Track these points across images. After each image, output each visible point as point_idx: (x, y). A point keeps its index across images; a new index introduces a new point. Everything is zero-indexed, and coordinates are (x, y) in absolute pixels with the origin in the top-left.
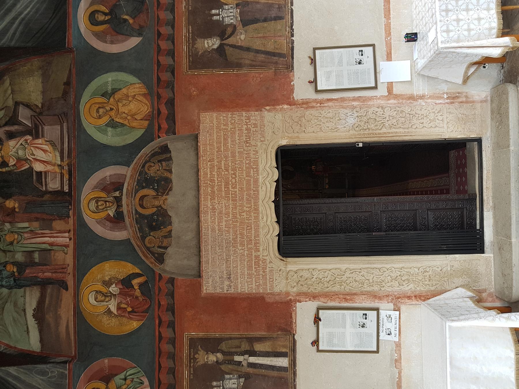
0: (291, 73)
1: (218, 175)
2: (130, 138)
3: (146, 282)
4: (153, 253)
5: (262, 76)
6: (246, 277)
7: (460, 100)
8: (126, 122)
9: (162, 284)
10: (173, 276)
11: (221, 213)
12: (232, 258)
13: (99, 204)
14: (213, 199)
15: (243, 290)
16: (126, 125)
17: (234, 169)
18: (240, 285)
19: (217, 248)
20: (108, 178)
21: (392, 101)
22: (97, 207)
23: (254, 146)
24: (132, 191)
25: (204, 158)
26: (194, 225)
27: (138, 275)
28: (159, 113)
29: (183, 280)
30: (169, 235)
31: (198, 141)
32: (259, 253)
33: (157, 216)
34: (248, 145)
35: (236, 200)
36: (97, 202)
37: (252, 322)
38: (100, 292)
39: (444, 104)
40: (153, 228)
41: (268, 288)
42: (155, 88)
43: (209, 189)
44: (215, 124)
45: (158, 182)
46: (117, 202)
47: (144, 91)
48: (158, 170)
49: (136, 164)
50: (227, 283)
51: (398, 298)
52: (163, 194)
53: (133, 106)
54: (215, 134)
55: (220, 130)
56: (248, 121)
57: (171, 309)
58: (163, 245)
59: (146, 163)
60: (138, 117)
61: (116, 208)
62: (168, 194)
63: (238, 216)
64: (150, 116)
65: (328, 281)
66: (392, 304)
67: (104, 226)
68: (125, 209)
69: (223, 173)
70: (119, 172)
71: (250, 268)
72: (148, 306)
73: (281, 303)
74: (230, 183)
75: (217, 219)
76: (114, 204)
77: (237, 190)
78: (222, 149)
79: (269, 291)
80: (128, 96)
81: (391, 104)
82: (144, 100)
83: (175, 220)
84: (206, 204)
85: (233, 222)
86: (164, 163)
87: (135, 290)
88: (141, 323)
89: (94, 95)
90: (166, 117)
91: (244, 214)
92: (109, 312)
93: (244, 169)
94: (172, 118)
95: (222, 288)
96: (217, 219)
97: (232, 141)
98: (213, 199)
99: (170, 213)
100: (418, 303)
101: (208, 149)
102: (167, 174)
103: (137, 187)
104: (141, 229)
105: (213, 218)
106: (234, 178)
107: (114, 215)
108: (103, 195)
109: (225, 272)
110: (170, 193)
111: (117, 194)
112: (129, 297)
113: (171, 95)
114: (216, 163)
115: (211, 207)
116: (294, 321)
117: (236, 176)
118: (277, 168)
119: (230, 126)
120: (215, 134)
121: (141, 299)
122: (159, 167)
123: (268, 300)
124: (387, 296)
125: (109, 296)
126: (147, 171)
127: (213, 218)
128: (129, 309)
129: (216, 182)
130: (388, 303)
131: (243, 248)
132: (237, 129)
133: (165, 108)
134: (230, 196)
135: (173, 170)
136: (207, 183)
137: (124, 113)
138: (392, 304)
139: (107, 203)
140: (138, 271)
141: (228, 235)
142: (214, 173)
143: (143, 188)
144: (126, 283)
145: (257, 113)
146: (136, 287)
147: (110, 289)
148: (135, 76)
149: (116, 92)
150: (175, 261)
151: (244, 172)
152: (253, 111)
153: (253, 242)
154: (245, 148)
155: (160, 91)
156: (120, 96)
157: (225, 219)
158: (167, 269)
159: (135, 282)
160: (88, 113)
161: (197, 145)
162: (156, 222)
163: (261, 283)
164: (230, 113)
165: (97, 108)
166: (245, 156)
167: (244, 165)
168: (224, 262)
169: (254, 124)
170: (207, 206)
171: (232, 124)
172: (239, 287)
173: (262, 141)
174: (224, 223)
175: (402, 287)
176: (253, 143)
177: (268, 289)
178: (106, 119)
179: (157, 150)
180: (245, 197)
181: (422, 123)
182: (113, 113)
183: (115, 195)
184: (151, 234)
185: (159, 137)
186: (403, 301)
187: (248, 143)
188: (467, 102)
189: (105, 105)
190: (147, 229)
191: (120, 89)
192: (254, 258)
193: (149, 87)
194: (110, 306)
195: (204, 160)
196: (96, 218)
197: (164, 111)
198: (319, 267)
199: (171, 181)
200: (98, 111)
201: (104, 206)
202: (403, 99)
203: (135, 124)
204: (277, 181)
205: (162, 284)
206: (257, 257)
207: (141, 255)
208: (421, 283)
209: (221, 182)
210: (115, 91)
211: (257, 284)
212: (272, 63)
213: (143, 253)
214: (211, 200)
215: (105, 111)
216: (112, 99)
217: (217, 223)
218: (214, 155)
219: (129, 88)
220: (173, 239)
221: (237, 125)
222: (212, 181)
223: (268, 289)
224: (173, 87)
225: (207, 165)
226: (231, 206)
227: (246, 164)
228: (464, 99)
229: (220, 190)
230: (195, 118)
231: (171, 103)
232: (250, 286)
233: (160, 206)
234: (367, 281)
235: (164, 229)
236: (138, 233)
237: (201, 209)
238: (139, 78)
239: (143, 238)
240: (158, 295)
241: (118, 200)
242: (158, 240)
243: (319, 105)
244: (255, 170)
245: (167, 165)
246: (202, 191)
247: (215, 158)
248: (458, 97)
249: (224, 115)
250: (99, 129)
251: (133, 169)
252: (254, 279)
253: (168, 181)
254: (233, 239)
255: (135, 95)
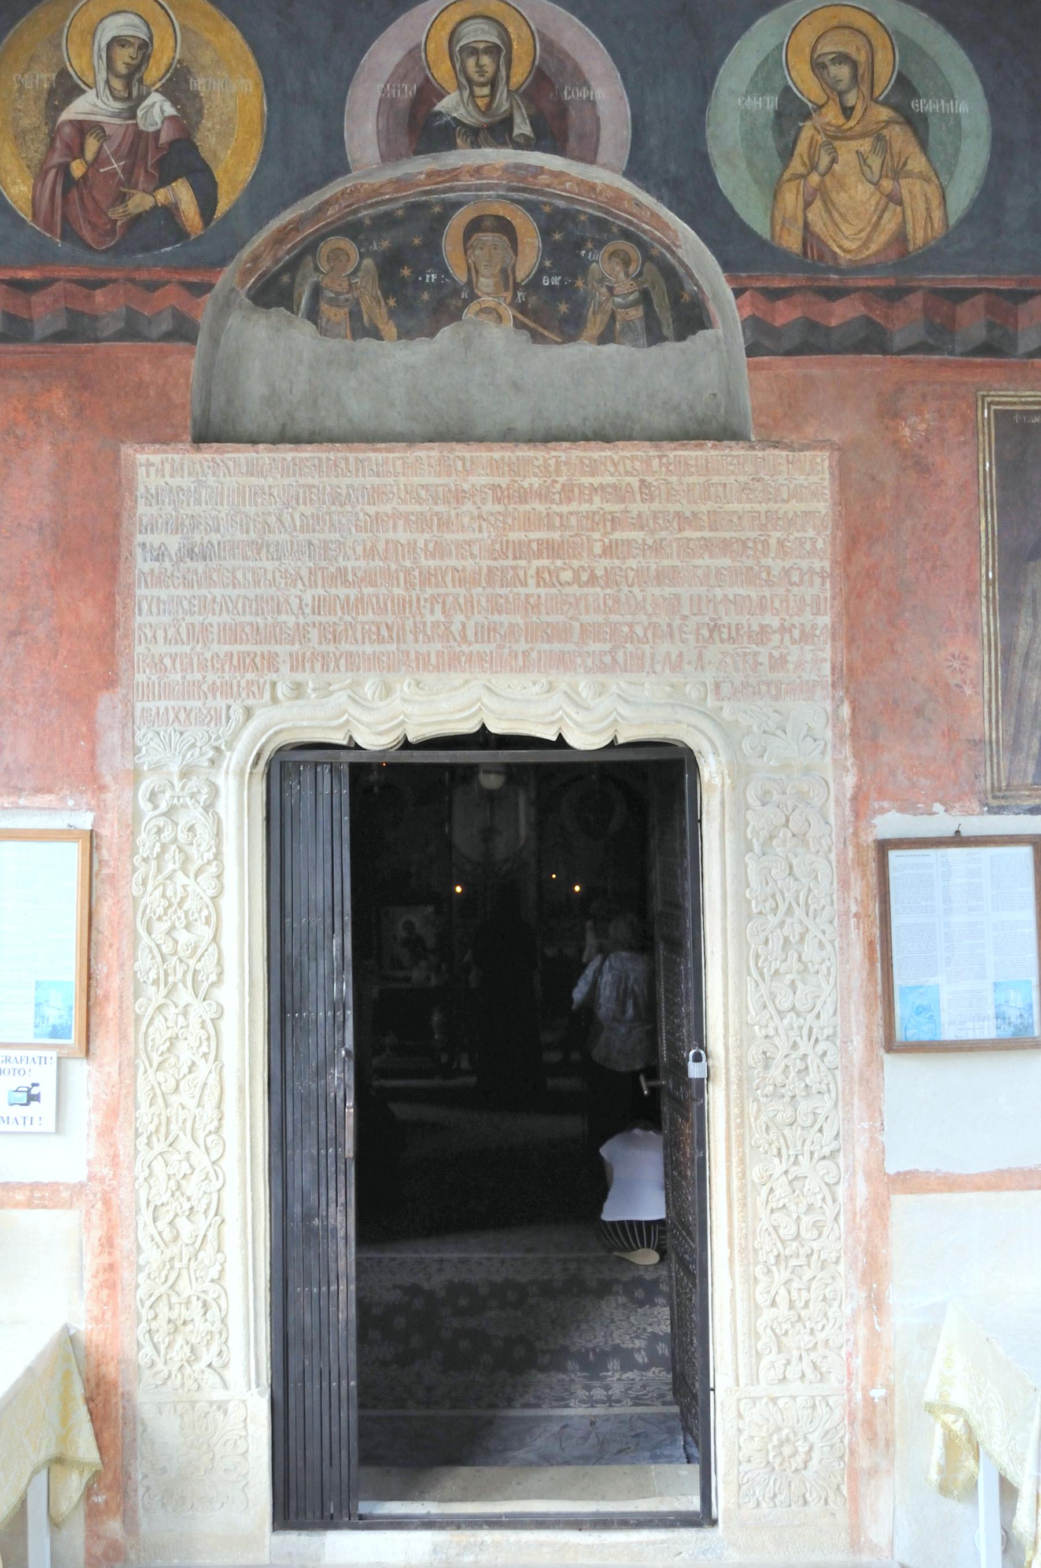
0: (975, 806)
1: (590, 516)
2: (736, 183)
3: (181, 234)
4: (293, 266)
5: (968, 691)
6: (197, 619)
7: (863, 1449)
8: (796, 165)
9: (171, 297)
10: (202, 339)
11: (444, 524)
12: (270, 565)
13: (486, 60)
14: (499, 494)
15: (145, 606)
16: (786, 166)
17: (610, 578)
18: (163, 594)
19: (308, 510)
20: (583, 94)
21: (862, 1189)
22: (475, 52)
23: (700, 657)
24: (532, 191)
25: (655, 462)
26: (396, 420)
27: (207, 199)
28: (832, 294)
29: (187, 376)
30: (362, 329)
31: (720, 440)
32: (285, 669)
33: (439, 285)
34: (706, 633)
35: (490, 583)
36: (493, 50)
37: (21, 640)
38: (145, 59)
39: (849, 1390)
40: (389, 270)
41: (152, 705)
42: (928, 280)
43: (536, 482)
44: (786, 507)
45: (565, 291)
46: (491, 129)
47: (918, 237)
48: (611, 289)
49: (638, 204)
50: (173, 542)
51: (107, 1203)
52: (522, 308)
53: (858, 195)
54: (748, 507)
55: (763, 527)
56: (796, 633)
57: (77, 330)
58: (324, 306)
59: (640, 244)
60: (816, 214)
61: (468, 120)
62: (519, 325)
63: (429, 591)
64: (821, 257)
65: (175, 934)
66: (83, 1178)
67: (400, 75)
68: (463, 157)
69: (596, 535)
70: (606, 134)
71: (232, 633)
72: (90, 241)
73: (93, 754)
74: (559, 563)
75: (417, 508)
76: (484, 114)
77: (532, 589)
78: (688, 534)
79: (139, 705)
80: (897, 173)
81: (851, 1187)
82: (881, 239)
83: (419, 352)
84: (479, 466)
85: (408, 572)
86: (637, 313)
87: (152, 193)
88: (25, 213)
89: (907, 48)
90: (822, 315)
91: (438, 616)
92: (67, 89)
93: (614, 618)
94: (812, 341)
95: (153, 528)
96: (417, 508)
97: (718, 571)
98: (499, 494)
99: (446, 332)
100: (87, 1274)
101: (691, 480)
102: (595, 326)
103: (547, 209)
104: (386, 222)
105: (423, 493)
106: (576, 580)
107: (439, 114)
108: (520, 73)
109: (215, 537)
110: (524, 336)
111: (522, 127)
112: (124, 169)
113: (898, 341)
114: (637, 507)
115: (466, 487)
116: (22, 802)
117: (586, 584)
118: (612, 745)
119: (777, 566)
120: (748, 507)
121: (117, 213)
122: (625, 296)
123: (104, 700)
124: (115, 1161)
125: (131, 86)
126: (610, 248)
127: (423, 493)
128: (77, 169)
129: (564, 509)
130: (89, 1163)
131: (308, 610)
132: (767, 592)
133: (851, 315)
134: (510, 562)
135: (611, 348)
136: (558, 472)
137: (834, 161)
138: (83, 1178)
139: (486, 91)
140: (223, 206)
141: (359, 550)
142: (597, 499)
143: (545, 233)
144: (181, 157)
145: (827, 667)
146: (162, 196)
147: (155, 98)
148: (976, 203)
149: (916, 133)
150: (271, 352)
151: (600, 618)
152: (834, 653)
153: (331, 648)
154: (691, 624)
155: (916, 301)
156: (897, 146)
157: (421, 539)
158: (234, 320)
159: (182, 194)
160: (835, 22)
161: (707, 438)
162: (409, 273)
163: (172, 677)
164: (827, 564)
165: (854, 55)
166: (663, 620)
167: (629, 618)
168: (253, 535)
169: (783, 660)
170: (468, 472)
171: (787, 572)
172: (156, 592)
173: (717, 686)
174: (402, 536)
175: (146, 1215)
176: (713, 652)
177: (146, 705)
178: (808, 86)
179: (690, 287)
180: (504, 618)
181: (773, 1304)
182: (832, 115)
183: (518, 120)
184: (368, 262)
185: (738, 293)
186: (95, 1218)
187: (711, 632)
188: (853, 1475)
189: (865, 88)
190: (386, 244)
191: (924, 146)
192: (266, 648)
193: (932, 256)
194: (90, 95)
195: (648, 460)
196: (431, 46)
197: (842, 313)
198: (230, 904)
199: (569, 338)
200: (842, 58)
201: (476, 77)
202: (869, 1230)
203: (791, 199)
204: (561, 743)
205: (171, 297)
206: (271, 662)
207: (288, 216)
208: (163, 1289)
209: (563, 527)
210: (917, 125)
211: (167, 661)
212: (1018, 730)
213: (297, 225)
214: (494, 487)
215: (842, 86)
216: (885, 113)
217: (403, 508)
218: (668, 500)
219: (928, 181)
220: (349, 342)
221: (781, 591)
222: (568, 493)
223: (146, 705)
224: (930, 349)
225: (627, 473)
226: (469, 563)
227: (631, 625)
228: (864, 1463)
229: (528, 522)
230: (809, 431)
231: (870, 340)
232: (160, 634)
233: (473, 297)
234: (172, 1083)
235: (384, 310)
236: (371, 211)
237: (461, 450)
238: (968, 218)
239: (352, 230)
240: (133, 281)
241: (498, 132)
242: (345, 284)
243: (854, 909)
244: (608, 659)
245: (628, 324)
246: (525, 452)
247: (656, 506)
248: (872, 1438)
249: (820, 544)
250: (772, 64)
251: (618, 190)
252: (187, 649)
253: (570, 328)
254: (342, 572)
255: (900, 203)
